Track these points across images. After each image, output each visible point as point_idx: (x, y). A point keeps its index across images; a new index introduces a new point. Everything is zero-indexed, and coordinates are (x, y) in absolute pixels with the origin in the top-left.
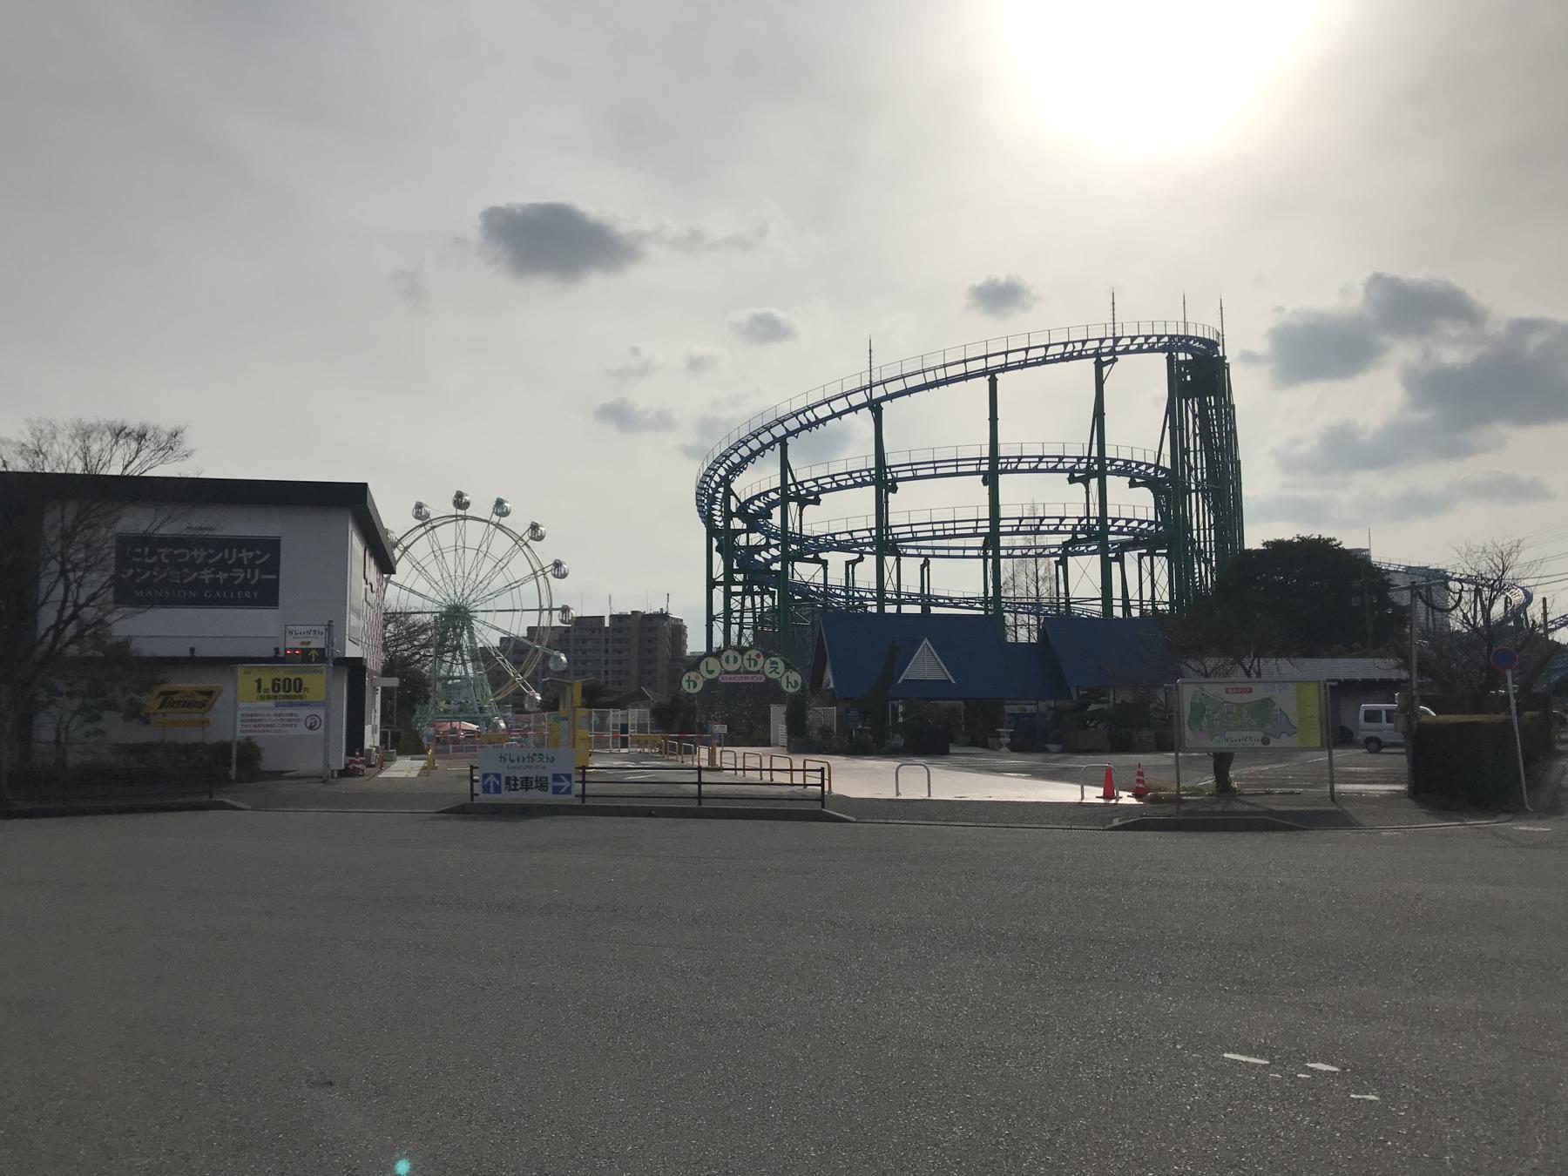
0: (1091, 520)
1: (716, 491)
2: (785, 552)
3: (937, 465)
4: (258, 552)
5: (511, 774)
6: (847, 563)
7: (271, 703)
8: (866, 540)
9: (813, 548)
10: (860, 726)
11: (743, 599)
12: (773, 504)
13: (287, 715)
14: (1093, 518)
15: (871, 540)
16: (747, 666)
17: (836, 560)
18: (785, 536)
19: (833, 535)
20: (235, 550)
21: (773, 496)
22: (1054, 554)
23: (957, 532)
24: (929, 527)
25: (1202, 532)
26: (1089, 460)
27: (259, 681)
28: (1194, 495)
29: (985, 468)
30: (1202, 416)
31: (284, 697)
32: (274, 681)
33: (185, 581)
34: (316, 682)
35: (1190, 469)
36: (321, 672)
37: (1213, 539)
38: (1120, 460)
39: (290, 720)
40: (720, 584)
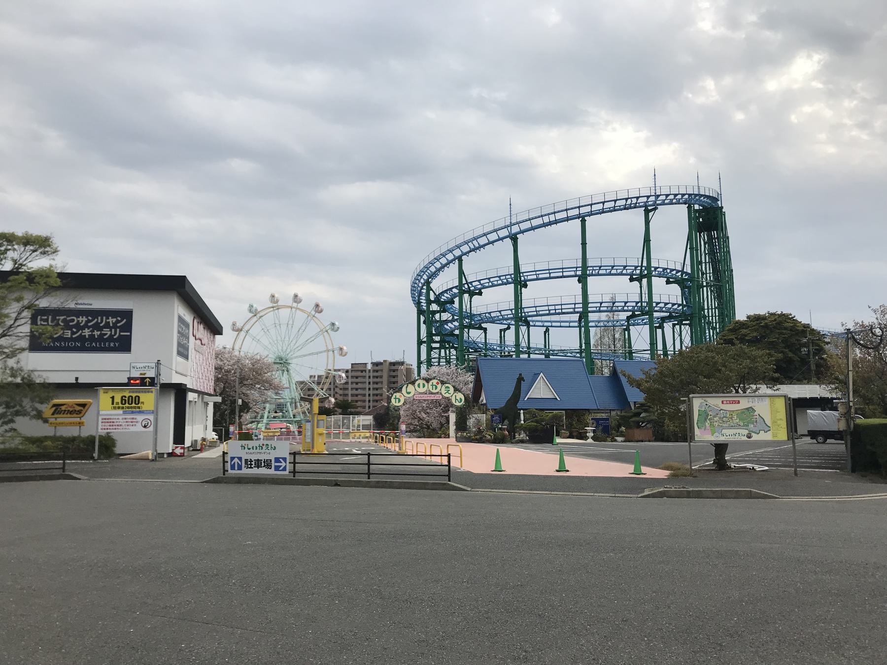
0: (643, 303)
1: (422, 288)
2: (461, 324)
3: (551, 271)
4: (119, 319)
5: (249, 457)
6: (501, 330)
7: (120, 412)
8: (509, 316)
9: (477, 322)
10: (500, 426)
11: (440, 352)
12: (455, 296)
13: (130, 419)
14: (644, 302)
15: (512, 316)
16: (431, 390)
17: (493, 330)
18: (461, 315)
19: (490, 313)
20: (104, 318)
21: (455, 291)
22: (622, 325)
23: (563, 311)
24: (546, 308)
25: (710, 310)
26: (641, 268)
27: (113, 398)
28: (705, 288)
29: (579, 273)
30: (710, 242)
31: (128, 408)
32: (122, 397)
33: (74, 336)
34: (148, 399)
35: (703, 274)
36: (152, 392)
37: (717, 315)
38: (661, 268)
39: (132, 422)
40: (424, 342)
